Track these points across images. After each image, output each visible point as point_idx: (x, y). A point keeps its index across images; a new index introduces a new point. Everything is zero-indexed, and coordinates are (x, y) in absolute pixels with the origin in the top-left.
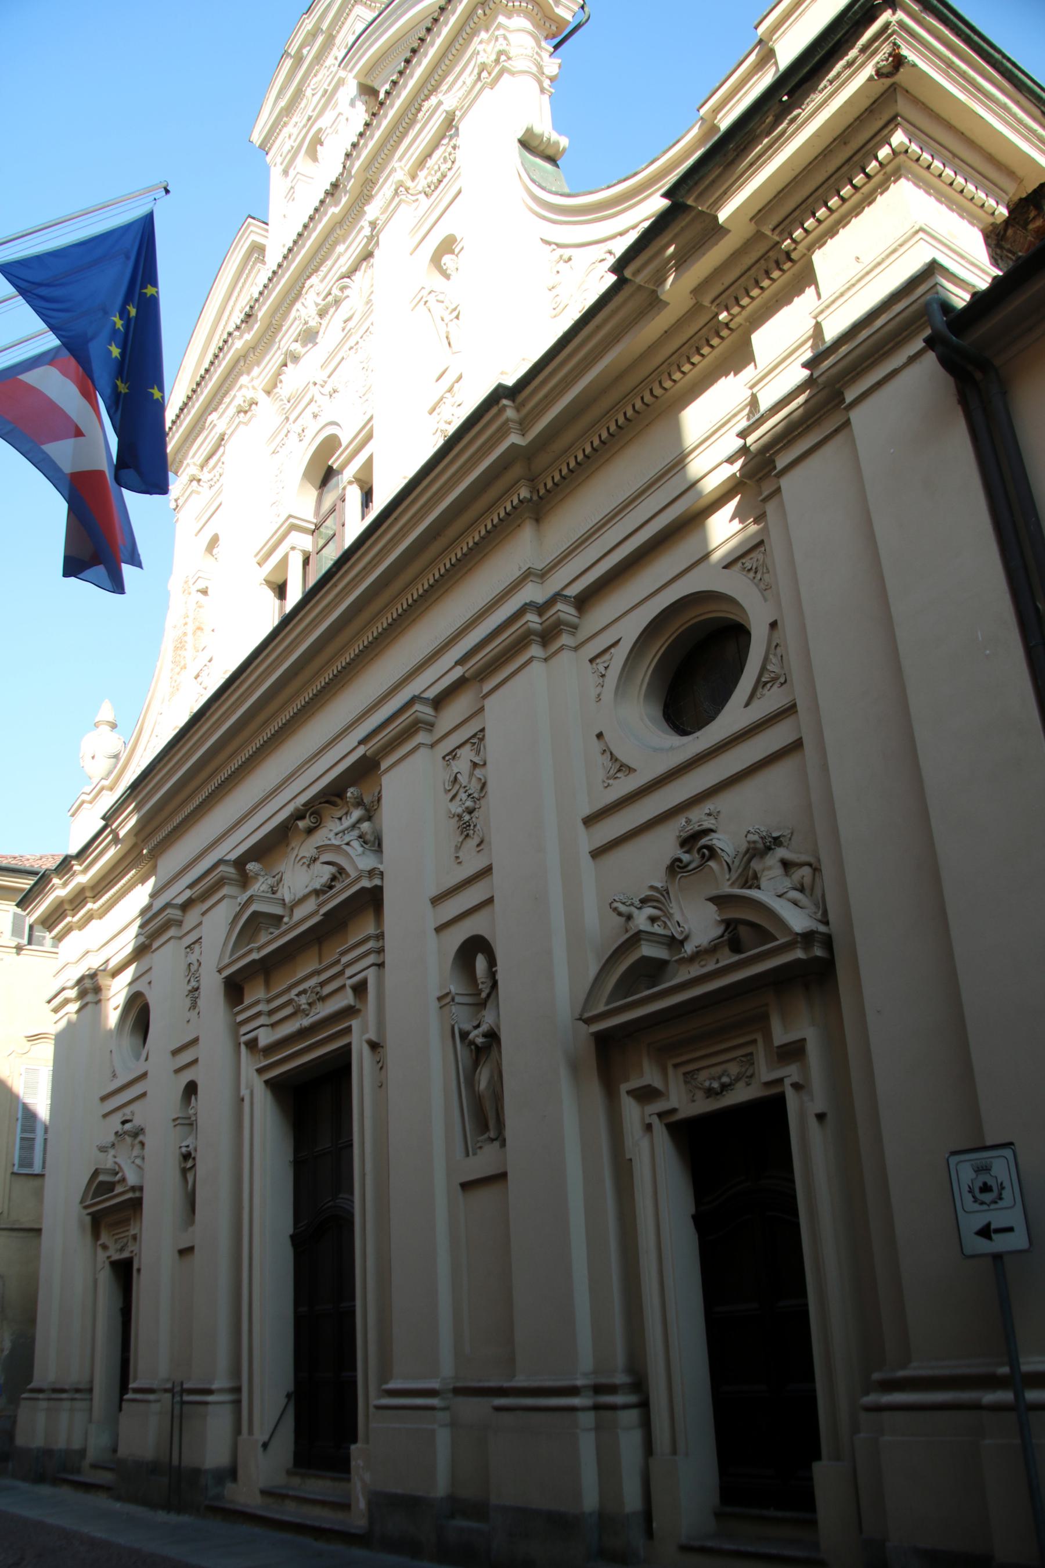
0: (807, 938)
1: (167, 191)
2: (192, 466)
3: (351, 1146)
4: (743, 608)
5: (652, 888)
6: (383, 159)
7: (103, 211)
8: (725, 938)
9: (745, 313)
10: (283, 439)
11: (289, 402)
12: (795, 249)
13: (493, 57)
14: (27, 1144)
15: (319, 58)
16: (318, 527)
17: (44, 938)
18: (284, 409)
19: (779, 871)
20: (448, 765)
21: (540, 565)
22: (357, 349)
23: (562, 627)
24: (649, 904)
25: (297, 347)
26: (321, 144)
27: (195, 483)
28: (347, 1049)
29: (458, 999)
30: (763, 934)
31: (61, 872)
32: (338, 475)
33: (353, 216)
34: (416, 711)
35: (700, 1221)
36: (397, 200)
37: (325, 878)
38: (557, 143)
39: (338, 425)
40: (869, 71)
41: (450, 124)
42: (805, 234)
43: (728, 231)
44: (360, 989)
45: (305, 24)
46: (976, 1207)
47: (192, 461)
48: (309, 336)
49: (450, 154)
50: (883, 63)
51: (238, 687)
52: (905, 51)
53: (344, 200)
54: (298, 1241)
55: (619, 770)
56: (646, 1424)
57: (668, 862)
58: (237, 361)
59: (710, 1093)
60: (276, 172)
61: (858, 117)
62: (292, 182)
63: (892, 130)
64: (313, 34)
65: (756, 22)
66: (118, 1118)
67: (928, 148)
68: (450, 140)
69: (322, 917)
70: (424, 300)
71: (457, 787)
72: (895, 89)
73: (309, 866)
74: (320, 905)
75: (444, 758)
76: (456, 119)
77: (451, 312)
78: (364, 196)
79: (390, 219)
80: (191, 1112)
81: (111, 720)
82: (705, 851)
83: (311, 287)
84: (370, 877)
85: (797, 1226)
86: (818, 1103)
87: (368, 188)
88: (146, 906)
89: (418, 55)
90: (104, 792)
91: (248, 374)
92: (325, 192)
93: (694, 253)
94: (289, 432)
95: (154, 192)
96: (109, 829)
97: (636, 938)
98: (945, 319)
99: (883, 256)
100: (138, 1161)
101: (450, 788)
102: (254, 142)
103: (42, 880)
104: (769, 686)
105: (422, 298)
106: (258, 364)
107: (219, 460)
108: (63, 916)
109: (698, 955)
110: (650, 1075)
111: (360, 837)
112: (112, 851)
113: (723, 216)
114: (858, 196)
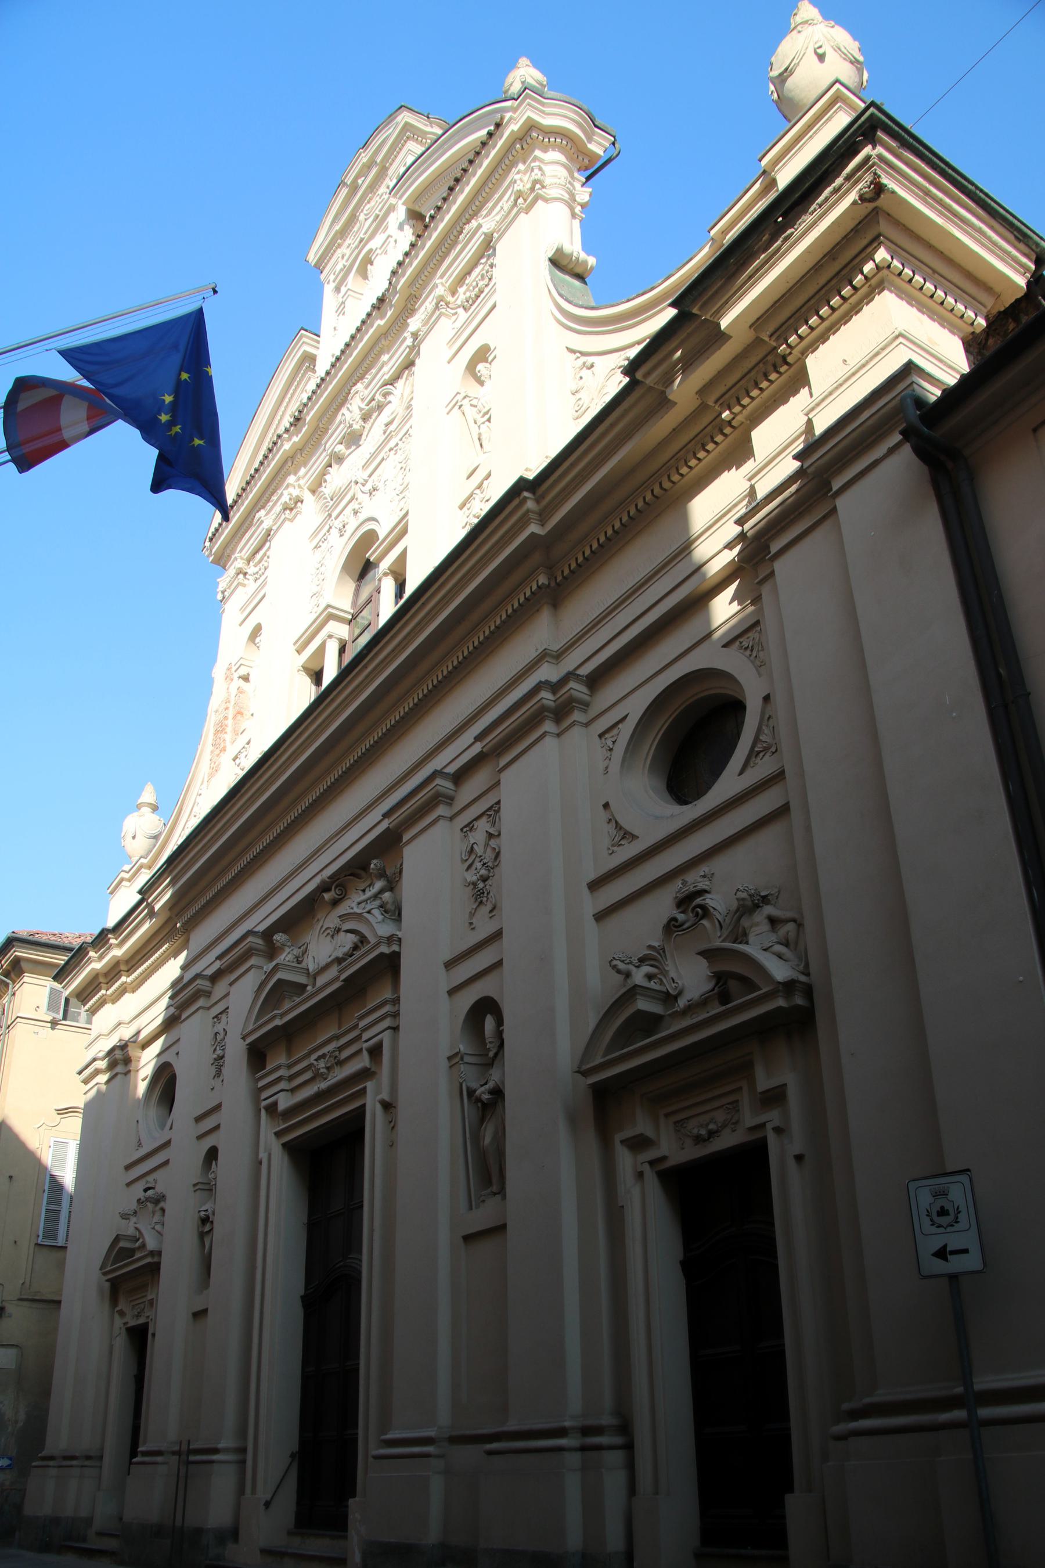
0: (789, 986)
1: (215, 292)
2: (239, 560)
3: (362, 1207)
4: (741, 685)
5: (650, 947)
6: (426, 276)
7: (156, 307)
8: (715, 991)
9: (746, 412)
10: (325, 534)
11: (332, 500)
12: (790, 353)
13: (529, 186)
14: (53, 1216)
15: (373, 187)
16: (354, 617)
17: (79, 1014)
18: (327, 507)
19: (765, 927)
20: (465, 836)
21: (555, 647)
22: (396, 450)
23: (574, 704)
24: (647, 963)
25: (341, 448)
26: (372, 264)
27: (241, 576)
28: (361, 1111)
29: (467, 1059)
30: (748, 984)
31: (97, 945)
32: (376, 568)
33: (397, 328)
34: (437, 785)
35: (690, 1267)
36: (437, 313)
37: (348, 946)
38: (585, 262)
39: (377, 521)
40: (853, 196)
41: (488, 246)
42: (799, 340)
43: (730, 337)
44: (375, 1052)
45: (360, 158)
46: (934, 1229)
47: (239, 555)
48: (353, 439)
49: (487, 272)
50: (865, 190)
51: (272, 765)
52: (885, 180)
53: (389, 313)
54: (308, 1302)
55: (623, 838)
56: (631, 1466)
57: (665, 921)
58: (285, 462)
59: (698, 1140)
60: (328, 289)
61: (845, 236)
62: (343, 298)
63: (875, 248)
64: (368, 166)
65: (760, 156)
66: (139, 1188)
67: (909, 263)
68: (488, 259)
69: (342, 983)
70: (459, 404)
71: (473, 857)
72: (877, 213)
73: (332, 937)
74: (341, 971)
75: (462, 830)
76: (494, 240)
77: (483, 416)
78: (408, 309)
79: (431, 330)
80: (211, 1176)
81: (153, 802)
82: (699, 909)
83: (357, 393)
84: (388, 944)
85: (776, 1267)
86: (796, 1145)
87: (412, 303)
88: (178, 978)
89: (461, 184)
90: (143, 870)
91: (295, 474)
92: (372, 306)
93: (699, 356)
94: (330, 528)
95: (203, 292)
96: (145, 903)
97: (633, 992)
98: (918, 412)
99: (867, 358)
100: (158, 1227)
101: (467, 858)
102: (310, 261)
103: (78, 955)
104: (761, 755)
105: (457, 402)
106: (305, 465)
107: (265, 554)
108: (97, 988)
109: (690, 1009)
110: (642, 1125)
111: (381, 906)
112: (147, 926)
113: (724, 323)
114: (846, 307)
